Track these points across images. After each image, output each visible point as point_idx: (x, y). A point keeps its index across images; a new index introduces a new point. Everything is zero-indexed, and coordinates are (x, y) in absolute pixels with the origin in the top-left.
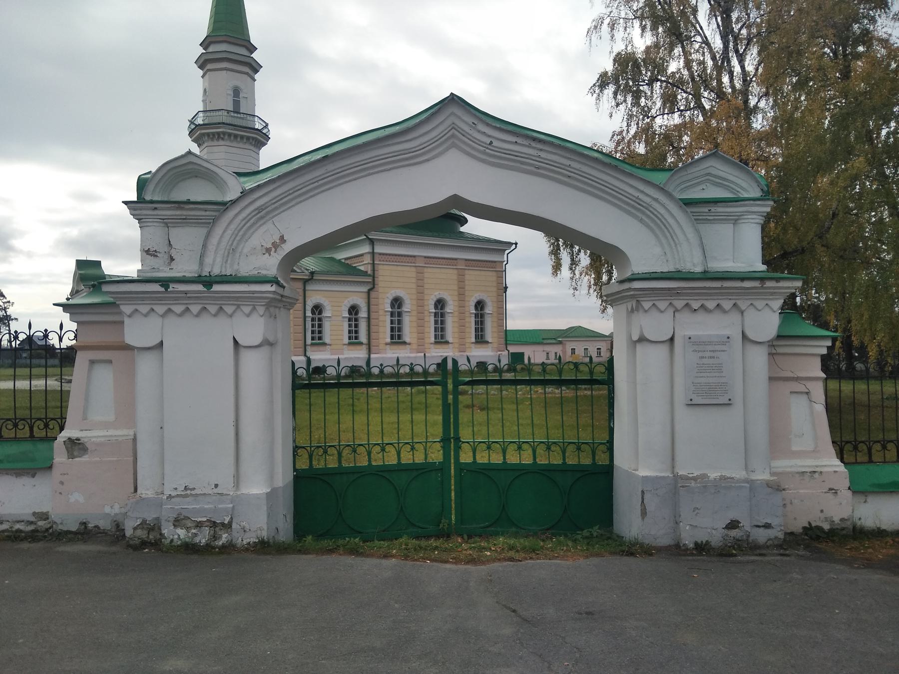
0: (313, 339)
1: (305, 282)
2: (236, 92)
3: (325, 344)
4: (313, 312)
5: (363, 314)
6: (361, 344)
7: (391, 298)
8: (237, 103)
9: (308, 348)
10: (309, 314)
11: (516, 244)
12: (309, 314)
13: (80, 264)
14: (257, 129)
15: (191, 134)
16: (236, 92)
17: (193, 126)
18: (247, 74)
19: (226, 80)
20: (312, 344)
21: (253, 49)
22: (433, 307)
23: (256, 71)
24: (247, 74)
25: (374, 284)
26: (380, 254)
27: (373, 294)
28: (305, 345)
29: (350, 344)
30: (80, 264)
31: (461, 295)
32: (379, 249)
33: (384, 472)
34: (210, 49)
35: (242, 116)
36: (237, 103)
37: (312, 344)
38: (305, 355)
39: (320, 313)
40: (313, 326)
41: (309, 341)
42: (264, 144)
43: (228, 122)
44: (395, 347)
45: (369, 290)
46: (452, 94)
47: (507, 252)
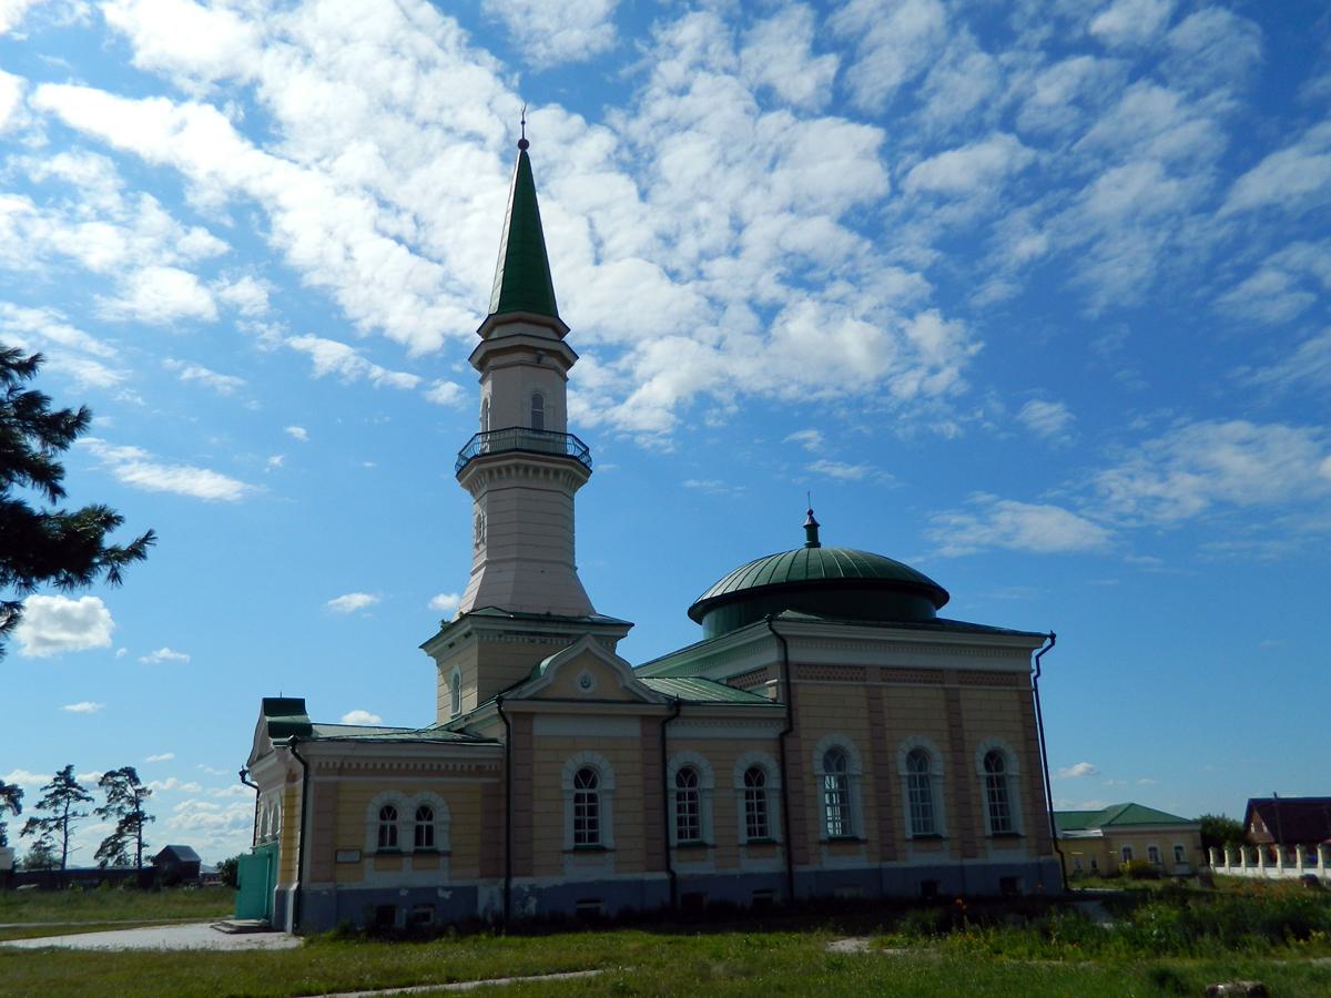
0: (681, 835)
1: (665, 722)
2: (537, 400)
3: (602, 850)
4: (680, 783)
5: (773, 782)
6: (771, 843)
7: (746, 767)
8: (537, 417)
9: (673, 854)
10: (672, 784)
11: (1053, 637)
12: (672, 784)
13: (271, 706)
14: (571, 457)
15: (460, 474)
16: (537, 400)
17: (463, 463)
18: (555, 369)
19: (525, 380)
20: (681, 847)
21: (562, 330)
22: (743, 781)
23: (569, 365)
24: (555, 369)
25: (791, 723)
26: (799, 665)
27: (790, 743)
28: (668, 848)
29: (751, 844)
30: (271, 706)
31: (957, 744)
32: (797, 655)
33: (223, 952)
34: (494, 335)
35: (547, 436)
36: (537, 417)
37: (681, 847)
38: (668, 869)
39: (693, 783)
40: (680, 809)
41: (674, 841)
42: (582, 482)
43: (525, 447)
44: (584, 858)
45: (782, 736)
46: (303, 700)
47: (1036, 652)
